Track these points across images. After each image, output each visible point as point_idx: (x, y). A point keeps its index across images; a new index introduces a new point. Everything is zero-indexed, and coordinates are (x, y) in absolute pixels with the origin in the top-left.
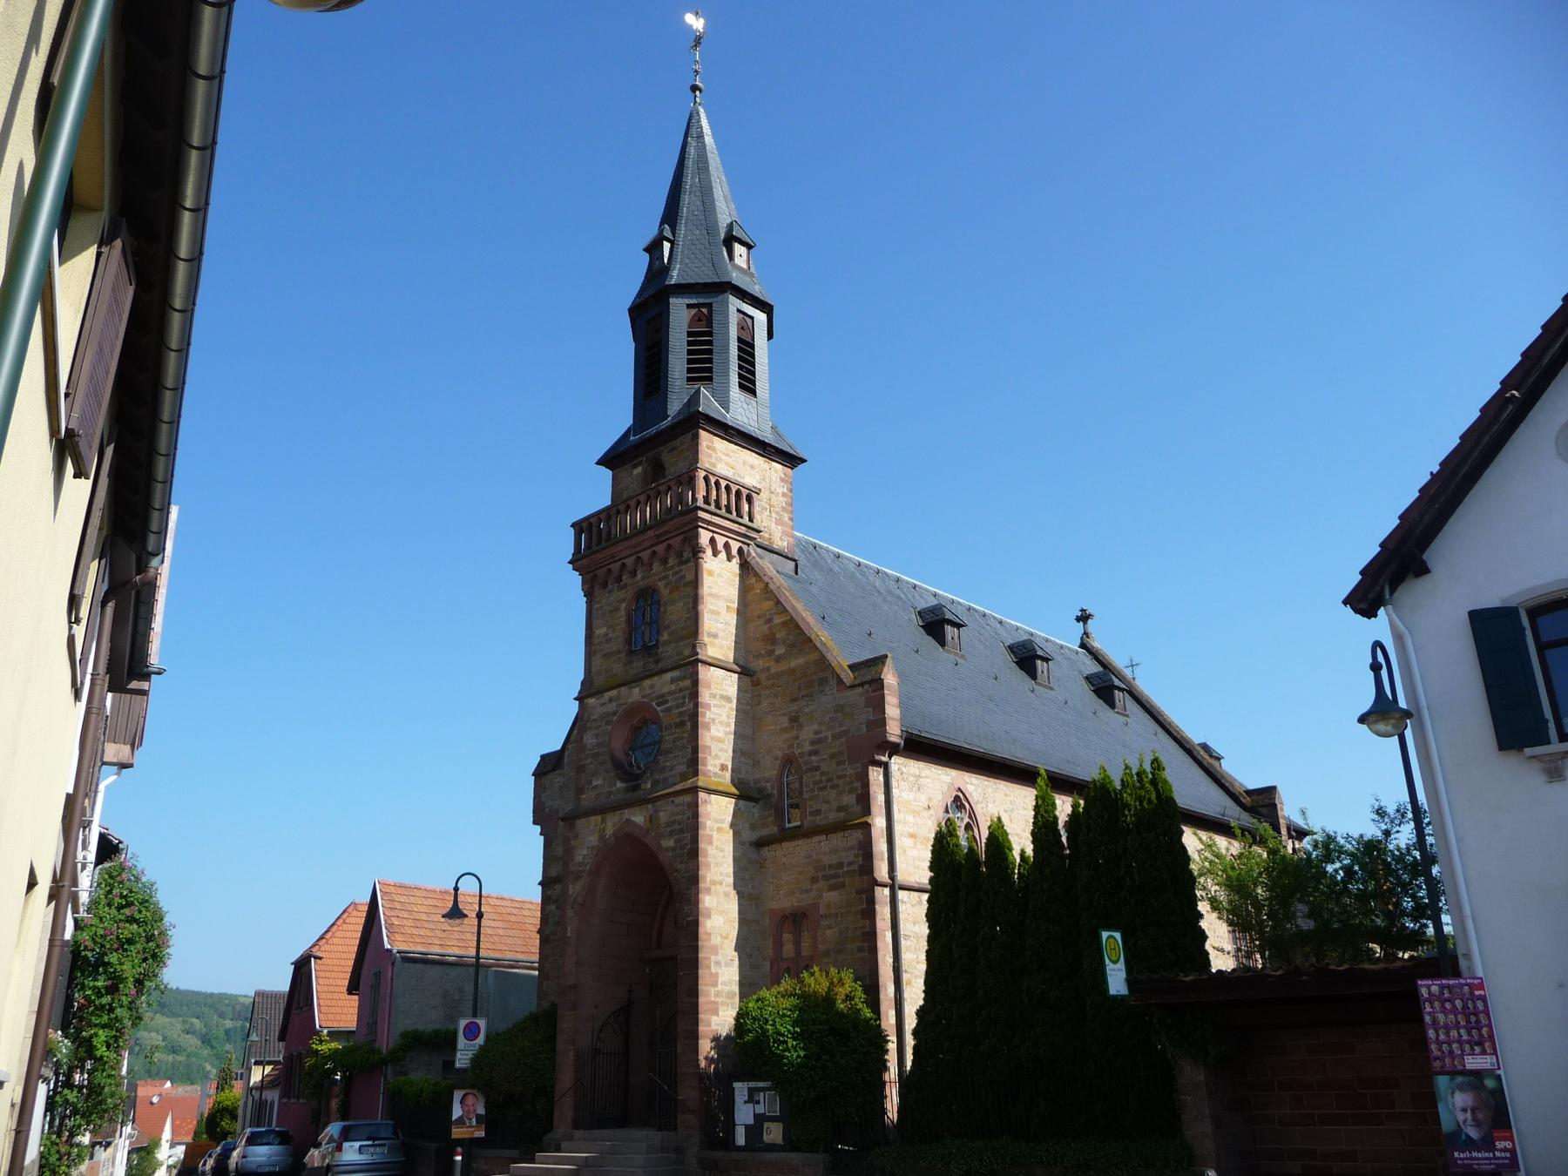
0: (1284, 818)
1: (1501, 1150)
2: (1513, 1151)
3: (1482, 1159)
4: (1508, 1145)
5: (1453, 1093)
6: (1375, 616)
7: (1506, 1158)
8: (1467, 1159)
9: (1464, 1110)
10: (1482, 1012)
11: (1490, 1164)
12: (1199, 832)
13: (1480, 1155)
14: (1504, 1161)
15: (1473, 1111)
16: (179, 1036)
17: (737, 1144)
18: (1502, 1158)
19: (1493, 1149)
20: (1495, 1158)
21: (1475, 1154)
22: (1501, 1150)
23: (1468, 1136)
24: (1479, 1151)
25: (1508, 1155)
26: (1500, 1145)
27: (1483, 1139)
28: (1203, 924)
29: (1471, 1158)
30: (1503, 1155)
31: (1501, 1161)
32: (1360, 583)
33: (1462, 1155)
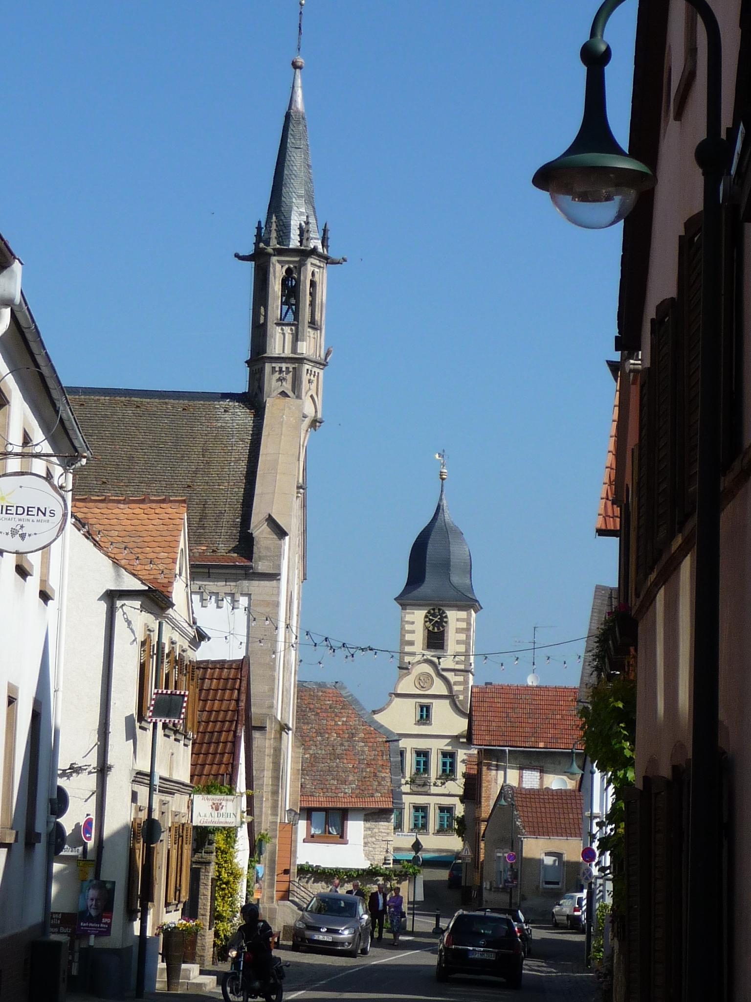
0: (605, 42)
1: (104, 923)
2: (110, 925)
3: (93, 927)
4: (108, 920)
5: (89, 889)
6: (617, 349)
7: (105, 928)
8: (86, 927)
9: (92, 899)
10: (160, 954)
11: (97, 930)
12: (94, 797)
13: (93, 925)
14: (104, 930)
15: (96, 900)
16: (270, 739)
17: (36, 831)
18: (103, 928)
19: (100, 922)
20: (100, 927)
21: (91, 925)
22: (104, 923)
23: (90, 914)
24: (93, 923)
25: (107, 926)
26: (104, 920)
27: (97, 916)
28: (37, 845)
29: (88, 927)
30: (104, 926)
31: (102, 929)
32: (705, 178)
33: (84, 925)
